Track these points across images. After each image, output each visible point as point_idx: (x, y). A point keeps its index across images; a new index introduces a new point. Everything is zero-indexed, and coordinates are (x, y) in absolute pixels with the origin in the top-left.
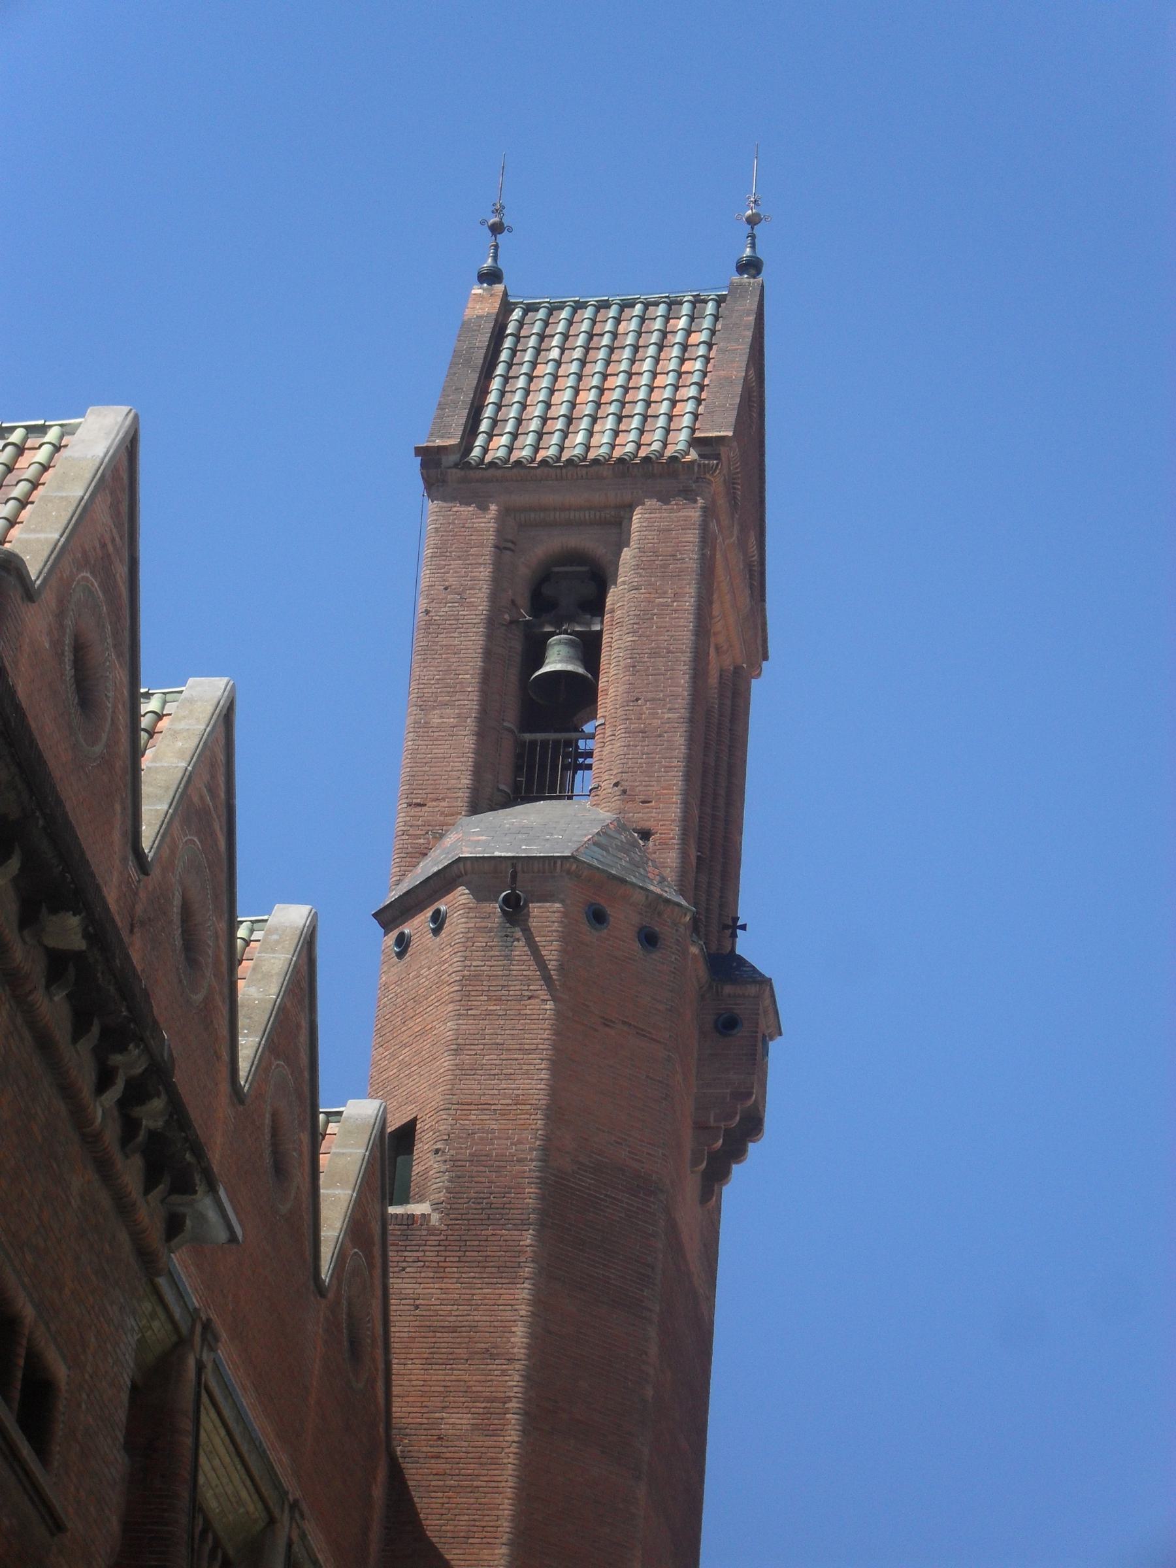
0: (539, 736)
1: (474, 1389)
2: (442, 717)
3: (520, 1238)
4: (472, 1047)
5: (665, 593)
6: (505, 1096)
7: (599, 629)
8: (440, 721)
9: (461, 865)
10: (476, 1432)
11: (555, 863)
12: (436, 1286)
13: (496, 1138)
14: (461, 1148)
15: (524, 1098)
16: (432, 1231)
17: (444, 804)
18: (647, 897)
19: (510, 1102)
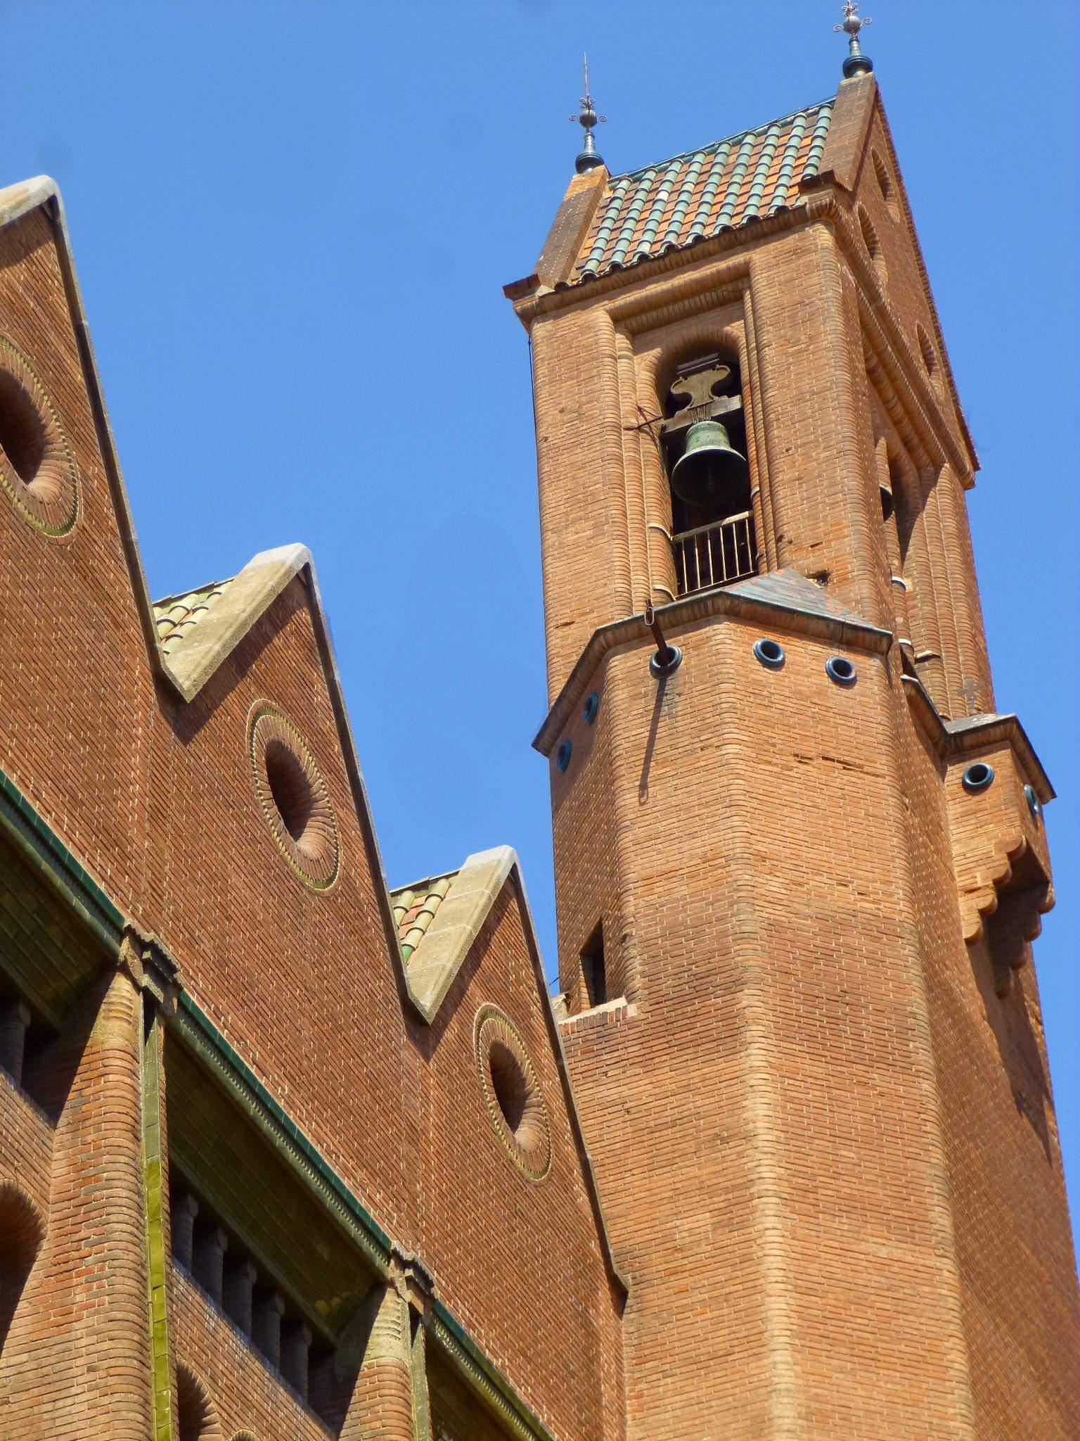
0: (694, 532)
1: (709, 1183)
2: (577, 533)
3: (733, 1002)
4: (646, 818)
5: (799, 340)
6: (691, 857)
7: (738, 406)
8: (576, 537)
9: (602, 638)
10: (720, 1231)
11: (705, 606)
12: (646, 1081)
13: (688, 903)
14: (650, 926)
15: (714, 852)
16: (632, 1024)
17: (595, 614)
18: (828, 626)
19: (699, 861)
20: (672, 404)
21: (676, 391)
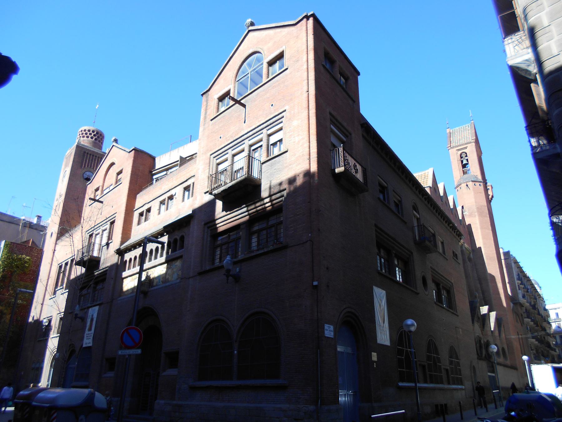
20: (461, 157)
21: (462, 156)
